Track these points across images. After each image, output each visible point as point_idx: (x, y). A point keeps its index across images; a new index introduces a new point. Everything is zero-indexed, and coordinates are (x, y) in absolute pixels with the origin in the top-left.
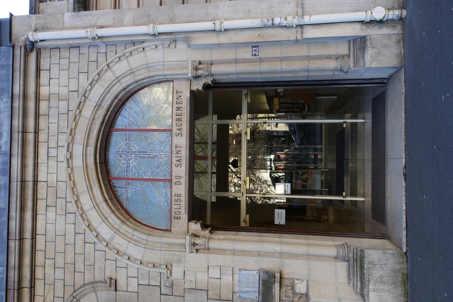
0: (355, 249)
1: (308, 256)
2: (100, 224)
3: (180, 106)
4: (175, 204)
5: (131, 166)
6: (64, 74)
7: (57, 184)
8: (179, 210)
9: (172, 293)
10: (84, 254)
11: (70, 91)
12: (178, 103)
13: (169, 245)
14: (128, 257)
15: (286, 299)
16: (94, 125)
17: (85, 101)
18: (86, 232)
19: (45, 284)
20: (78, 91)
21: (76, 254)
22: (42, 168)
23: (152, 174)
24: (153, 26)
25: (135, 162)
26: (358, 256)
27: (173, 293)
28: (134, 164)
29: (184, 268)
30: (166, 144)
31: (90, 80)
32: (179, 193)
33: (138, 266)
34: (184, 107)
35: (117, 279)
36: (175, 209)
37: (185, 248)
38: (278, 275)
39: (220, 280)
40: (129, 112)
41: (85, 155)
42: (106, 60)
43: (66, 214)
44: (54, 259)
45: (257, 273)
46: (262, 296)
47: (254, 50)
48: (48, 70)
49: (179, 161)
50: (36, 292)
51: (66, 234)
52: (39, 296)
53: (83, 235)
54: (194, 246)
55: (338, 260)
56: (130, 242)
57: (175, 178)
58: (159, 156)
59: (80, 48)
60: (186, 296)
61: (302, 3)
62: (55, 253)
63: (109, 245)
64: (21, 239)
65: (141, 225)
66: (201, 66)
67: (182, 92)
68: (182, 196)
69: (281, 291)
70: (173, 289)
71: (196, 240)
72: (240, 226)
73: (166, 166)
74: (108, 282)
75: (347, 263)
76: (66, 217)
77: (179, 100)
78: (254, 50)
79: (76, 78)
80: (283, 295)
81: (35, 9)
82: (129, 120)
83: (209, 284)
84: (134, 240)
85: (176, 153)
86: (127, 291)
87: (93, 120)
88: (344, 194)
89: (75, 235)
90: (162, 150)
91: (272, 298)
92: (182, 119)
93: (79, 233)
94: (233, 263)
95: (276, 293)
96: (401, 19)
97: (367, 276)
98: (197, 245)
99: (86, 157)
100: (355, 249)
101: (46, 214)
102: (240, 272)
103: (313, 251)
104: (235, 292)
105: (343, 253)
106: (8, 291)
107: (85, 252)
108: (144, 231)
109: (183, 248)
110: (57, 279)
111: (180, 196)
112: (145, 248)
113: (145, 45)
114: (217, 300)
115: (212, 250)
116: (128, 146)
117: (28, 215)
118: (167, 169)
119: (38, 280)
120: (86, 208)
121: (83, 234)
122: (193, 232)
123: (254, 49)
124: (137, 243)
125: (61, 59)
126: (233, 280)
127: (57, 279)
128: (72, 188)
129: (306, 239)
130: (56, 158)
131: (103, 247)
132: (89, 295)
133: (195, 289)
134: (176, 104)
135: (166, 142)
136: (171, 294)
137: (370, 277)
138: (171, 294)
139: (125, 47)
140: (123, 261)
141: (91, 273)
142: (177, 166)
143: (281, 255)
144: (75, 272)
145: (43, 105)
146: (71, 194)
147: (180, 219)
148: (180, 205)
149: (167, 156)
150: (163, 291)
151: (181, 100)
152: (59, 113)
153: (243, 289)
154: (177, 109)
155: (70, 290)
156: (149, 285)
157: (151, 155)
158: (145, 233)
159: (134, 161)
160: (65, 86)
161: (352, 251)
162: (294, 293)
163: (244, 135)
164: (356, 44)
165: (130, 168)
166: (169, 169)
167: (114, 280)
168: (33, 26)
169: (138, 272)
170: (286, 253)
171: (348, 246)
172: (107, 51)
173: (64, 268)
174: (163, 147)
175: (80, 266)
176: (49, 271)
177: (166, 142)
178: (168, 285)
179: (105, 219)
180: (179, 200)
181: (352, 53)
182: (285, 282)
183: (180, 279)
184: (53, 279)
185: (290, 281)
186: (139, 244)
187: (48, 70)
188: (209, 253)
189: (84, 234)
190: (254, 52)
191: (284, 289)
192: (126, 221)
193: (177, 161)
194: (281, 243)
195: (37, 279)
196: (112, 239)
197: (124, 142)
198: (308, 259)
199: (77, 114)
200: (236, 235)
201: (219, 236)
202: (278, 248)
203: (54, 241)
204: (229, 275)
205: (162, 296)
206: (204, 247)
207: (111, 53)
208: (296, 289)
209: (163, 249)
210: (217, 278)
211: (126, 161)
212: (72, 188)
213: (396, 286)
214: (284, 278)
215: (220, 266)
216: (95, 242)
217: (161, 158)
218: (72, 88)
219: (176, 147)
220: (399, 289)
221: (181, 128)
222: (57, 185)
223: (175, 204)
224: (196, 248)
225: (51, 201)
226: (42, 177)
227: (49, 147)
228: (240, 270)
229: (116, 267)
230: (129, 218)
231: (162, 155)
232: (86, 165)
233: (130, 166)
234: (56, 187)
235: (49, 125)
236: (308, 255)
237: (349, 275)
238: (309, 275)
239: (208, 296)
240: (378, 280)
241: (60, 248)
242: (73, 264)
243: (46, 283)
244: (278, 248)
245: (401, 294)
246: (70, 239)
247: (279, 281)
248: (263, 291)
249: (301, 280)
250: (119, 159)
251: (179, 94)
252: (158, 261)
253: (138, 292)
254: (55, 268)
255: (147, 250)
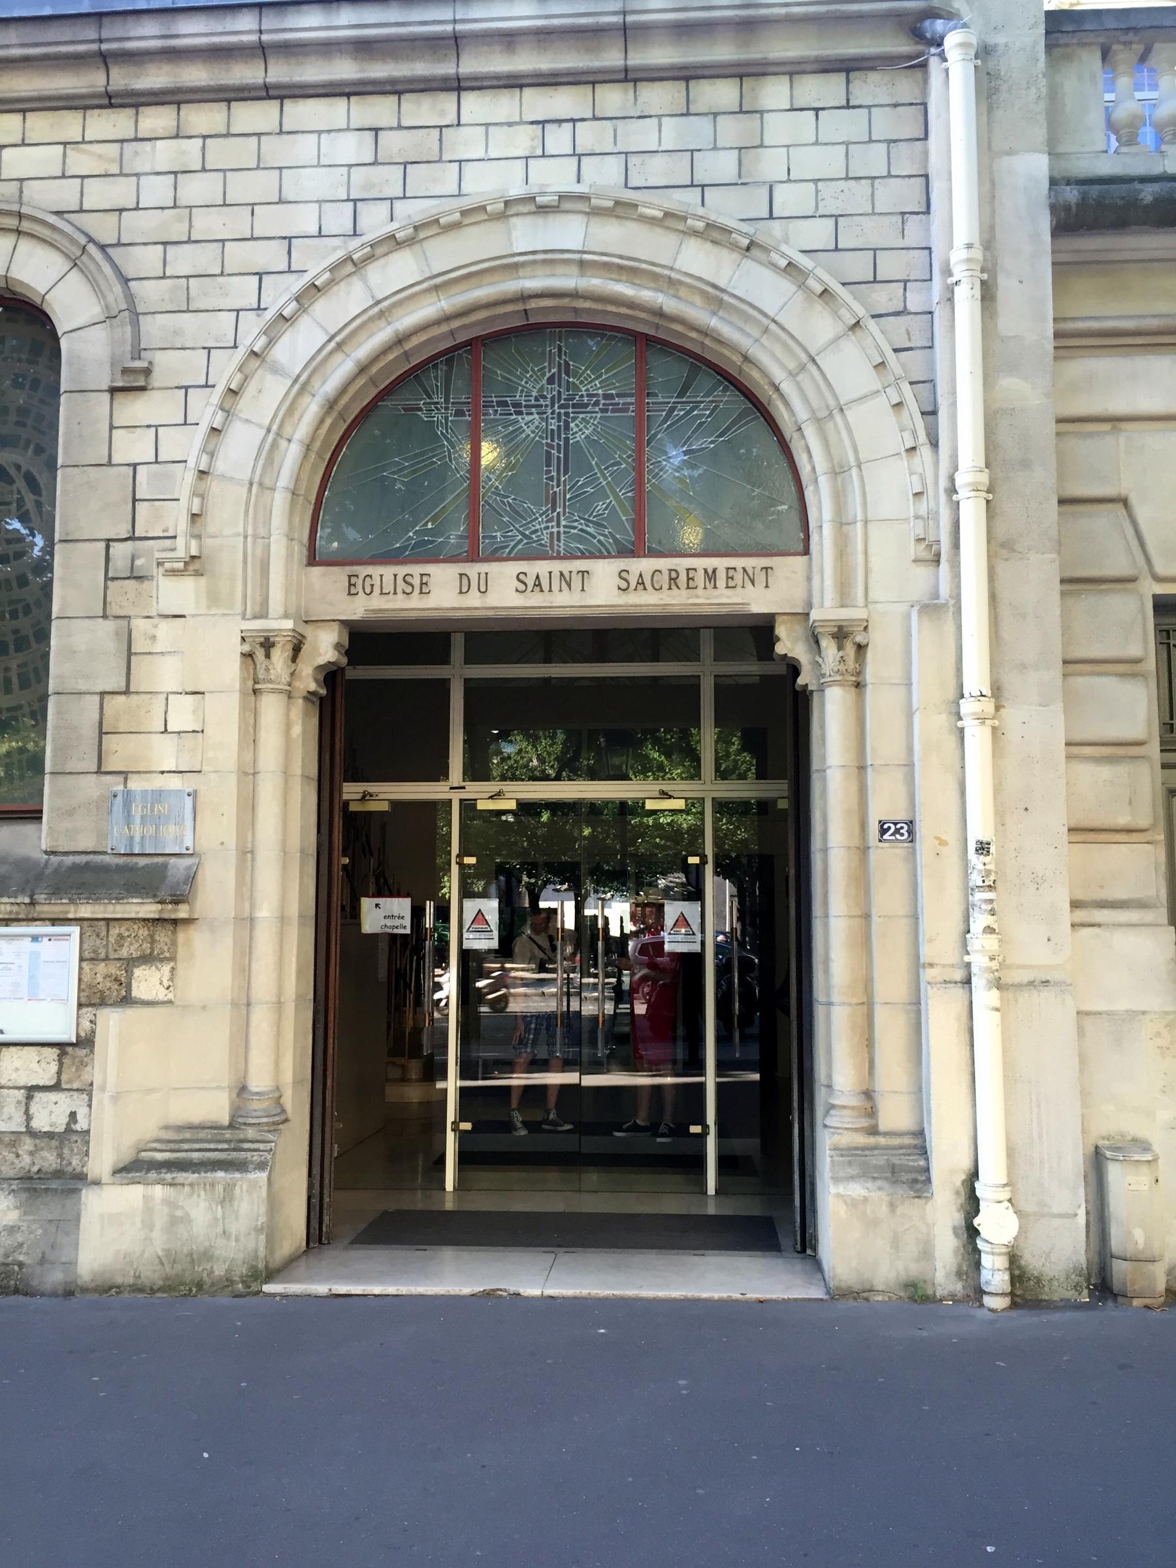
0: (268, 1146)
1: (244, 1005)
2: (322, 326)
3: (721, 582)
4: (395, 576)
5: (520, 417)
6: (830, 162)
7: (450, 161)
8: (377, 590)
9: (113, 579)
10: (222, 274)
11: (771, 187)
12: (731, 573)
13: (262, 561)
14: (220, 428)
15: (112, 939)
16: (652, 285)
17: (734, 246)
18: (295, 276)
19: (122, 141)
20: (771, 217)
21: (221, 244)
22: (502, 106)
23: (493, 493)
24: (980, 483)
25: (533, 432)
26: (249, 1154)
27: (116, 582)
28: (525, 427)
29: (193, 616)
30: (595, 537)
31: (805, 262)
32: (431, 586)
33: (191, 463)
34: (717, 597)
35: (147, 393)
36: (381, 576)
37: (255, 618)
38: (182, 912)
39: (162, 733)
40: (703, 402)
41: (550, 259)
42: (873, 317)
43: (352, 200)
44: (204, 170)
45: (187, 849)
46: (117, 865)
47: (898, 826)
48: (848, 100)
49: (538, 584)
50: (97, 111)
51: (285, 206)
52: (84, 126)
53: (283, 266)
54: (262, 645)
55: (234, 1095)
56: (269, 431)
57: (479, 574)
58: (555, 514)
59: (923, 213)
60: (107, 622)
61: (1047, 981)
62: (224, 171)
63: (255, 363)
64: (262, 51)
65: (326, 463)
66: (850, 650)
67: (767, 587)
68: (421, 599)
69: (135, 923)
70: (127, 581)
71: (282, 652)
72: (345, 781)
73: (521, 540)
74: (138, 364)
75: (226, 1122)
76: (343, 201)
77: (739, 576)
78: (898, 826)
79: (817, 207)
80: (123, 929)
81: (1074, 32)
82: (674, 403)
83: (149, 696)
84: (274, 445)
85: (562, 574)
86: (112, 427)
87: (671, 282)
88: (466, 1126)
89: (285, 238)
90: (576, 524)
91: (114, 895)
92: (675, 591)
93: (289, 253)
94: (216, 772)
95: (128, 907)
96: (980, 1292)
97: (189, 1181)
98: (268, 656)
99: (545, 261)
100: (268, 1146)
101: (348, 129)
102: (189, 795)
103: (261, 1021)
104: (126, 779)
105: (255, 1111)
106: (93, 19)
107: (229, 275)
108: (304, 477)
109: (257, 609)
110: (138, 184)
111: (421, 593)
112: (251, 484)
113: (925, 451)
114: (101, 724)
115: (253, 704)
116: (586, 406)
117: (345, 70)
118: (512, 544)
119: (134, 118)
120: (374, 273)
121: (290, 267)
122: (308, 639)
123: (902, 828)
124: (269, 454)
125: (885, 145)
126: (162, 772)
127: (138, 184)
128: (437, 221)
129: (299, 998)
130: (540, 152)
131: (248, 342)
132: (95, 300)
133: (130, 654)
134: (728, 569)
135: (602, 538)
136: (110, 575)
137: (187, 1189)
138: (110, 575)
139: (924, 382)
140: (205, 410)
141: (163, 300)
142: (522, 577)
143: (247, 922)
144: (165, 243)
145: (723, 93)
146: (418, 218)
147: (349, 594)
148: (395, 593)
149: (556, 542)
150: (116, 548)
151: (740, 583)
152: (696, 154)
153: (137, 806)
154: (710, 572)
155: (103, 227)
156: (134, 500)
157: (558, 486)
158: (298, 480)
159: (537, 427)
160: (789, 170)
161: (263, 1138)
162: (130, 963)
163: (658, 788)
164: (909, 1155)
165: (511, 414)
166: (510, 552)
167: (146, 381)
168: (999, 39)
169: (174, 462)
170: (251, 938)
171: (279, 1124)
172: (911, 316)
173: (175, 207)
174: (584, 527)
175: (184, 260)
176: (165, 154)
177: (602, 538)
178: (138, 562)
179: (339, 343)
180: (409, 590)
181: (882, 1141)
182: (162, 936)
183: (158, 602)
184: (138, 170)
185: (166, 948)
186: (261, 462)
187: (848, 100)
188: (243, 693)
189: (290, 271)
190: (893, 826)
191: (143, 932)
192: (335, 414)
193: (538, 577)
194: (283, 919)
195: (137, 113)
196: (276, 370)
197: (600, 392)
198: (234, 1004)
199: (689, 221)
200: (305, 777)
201: (300, 722)
202: (265, 912)
203: (262, 166)
204: (177, 760)
205: (103, 545)
206: (261, 677)
207: (903, 330)
208: (144, 967)
209: (249, 545)
210: (166, 721)
211: (536, 399)
212: (437, 221)
213: (162, 1263)
214: (174, 932)
215: (202, 731)
216: (265, 309)
217: (547, 522)
218: (780, 193)
219: (583, 572)
220: (155, 1271)
221: (645, 589)
222: (448, 164)
223: (395, 576)
224: (257, 652)
225: (393, 142)
226: (475, 105)
227: (578, 124)
228: (194, 795)
229: (187, 388)
230: (349, 421)
231: (558, 525)
232: (516, 266)
233: (520, 413)
234: (440, 161)
235: (653, 119)
236: (248, 1005)
237: (189, 1128)
238: (185, 1007)
239: (111, 696)
240: (179, 1213)
241: (242, 188)
242: (189, 237)
243: (125, 144)
244: (265, 912)
245: (139, 1276)
246: (270, 221)
247: (166, 916)
248: (132, 869)
249: (171, 984)
250: (544, 375)
251: (760, 578)
252: (211, 529)
253: (110, 464)
254: (173, 176)
255: (245, 489)
